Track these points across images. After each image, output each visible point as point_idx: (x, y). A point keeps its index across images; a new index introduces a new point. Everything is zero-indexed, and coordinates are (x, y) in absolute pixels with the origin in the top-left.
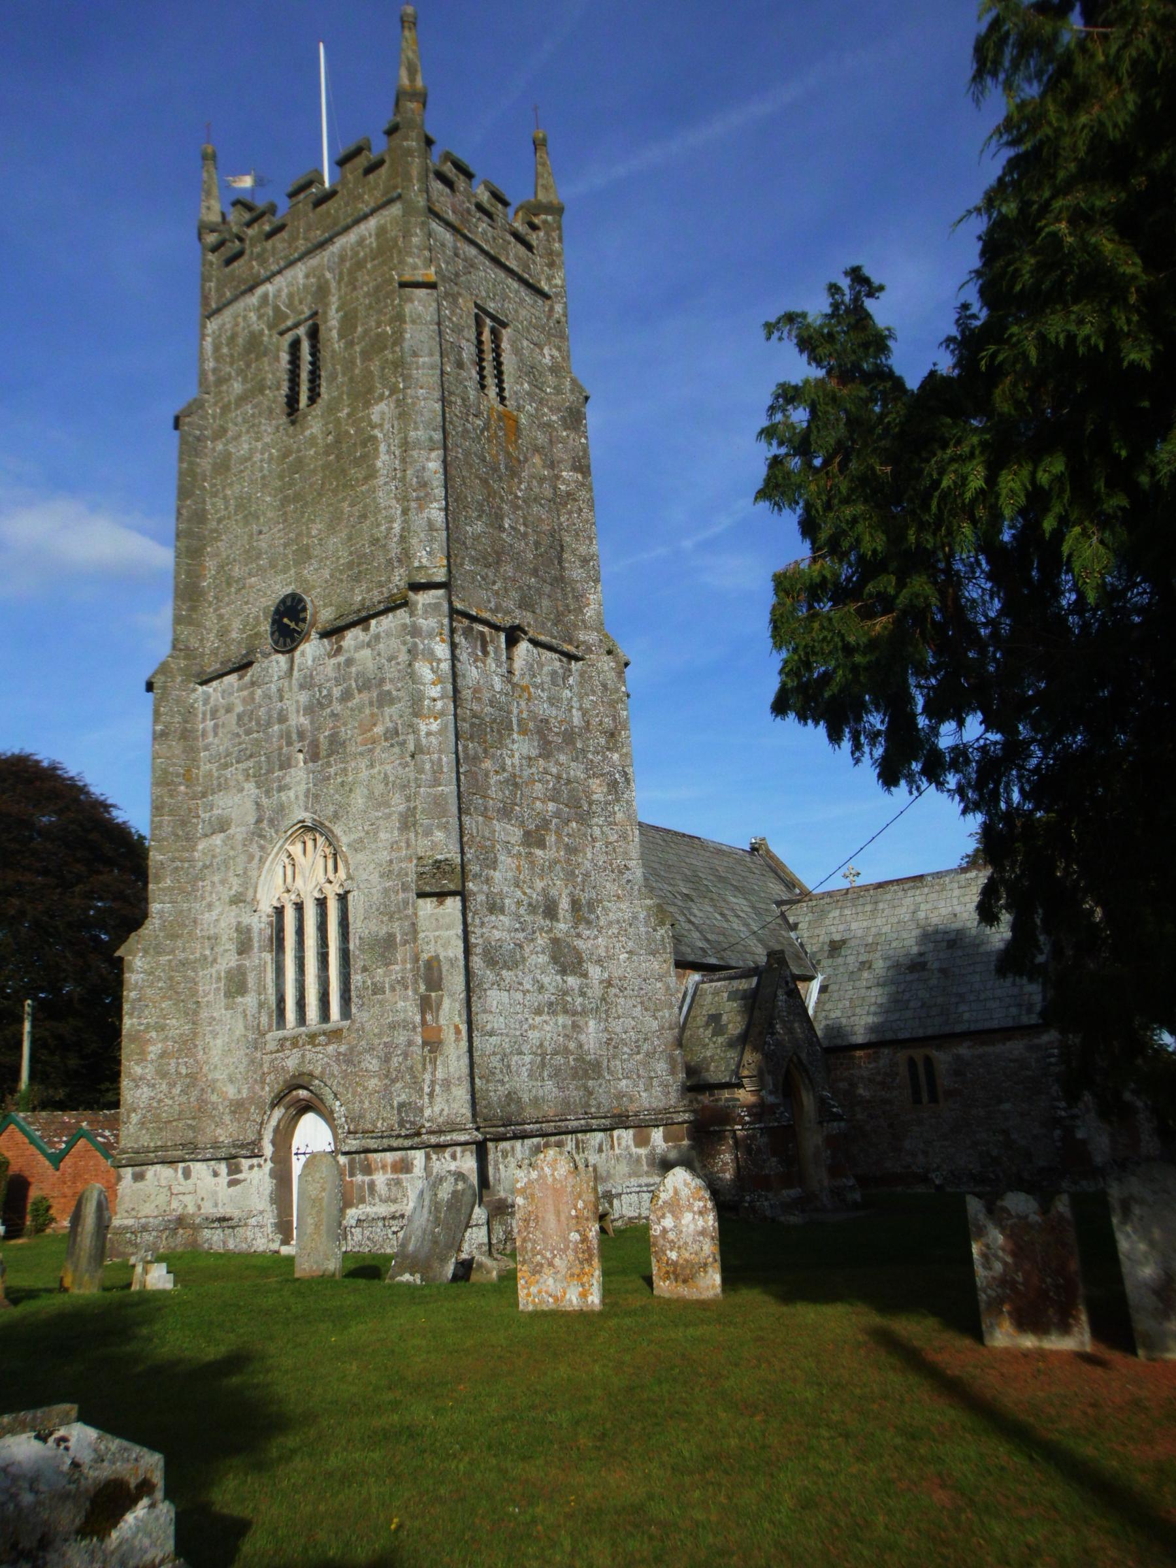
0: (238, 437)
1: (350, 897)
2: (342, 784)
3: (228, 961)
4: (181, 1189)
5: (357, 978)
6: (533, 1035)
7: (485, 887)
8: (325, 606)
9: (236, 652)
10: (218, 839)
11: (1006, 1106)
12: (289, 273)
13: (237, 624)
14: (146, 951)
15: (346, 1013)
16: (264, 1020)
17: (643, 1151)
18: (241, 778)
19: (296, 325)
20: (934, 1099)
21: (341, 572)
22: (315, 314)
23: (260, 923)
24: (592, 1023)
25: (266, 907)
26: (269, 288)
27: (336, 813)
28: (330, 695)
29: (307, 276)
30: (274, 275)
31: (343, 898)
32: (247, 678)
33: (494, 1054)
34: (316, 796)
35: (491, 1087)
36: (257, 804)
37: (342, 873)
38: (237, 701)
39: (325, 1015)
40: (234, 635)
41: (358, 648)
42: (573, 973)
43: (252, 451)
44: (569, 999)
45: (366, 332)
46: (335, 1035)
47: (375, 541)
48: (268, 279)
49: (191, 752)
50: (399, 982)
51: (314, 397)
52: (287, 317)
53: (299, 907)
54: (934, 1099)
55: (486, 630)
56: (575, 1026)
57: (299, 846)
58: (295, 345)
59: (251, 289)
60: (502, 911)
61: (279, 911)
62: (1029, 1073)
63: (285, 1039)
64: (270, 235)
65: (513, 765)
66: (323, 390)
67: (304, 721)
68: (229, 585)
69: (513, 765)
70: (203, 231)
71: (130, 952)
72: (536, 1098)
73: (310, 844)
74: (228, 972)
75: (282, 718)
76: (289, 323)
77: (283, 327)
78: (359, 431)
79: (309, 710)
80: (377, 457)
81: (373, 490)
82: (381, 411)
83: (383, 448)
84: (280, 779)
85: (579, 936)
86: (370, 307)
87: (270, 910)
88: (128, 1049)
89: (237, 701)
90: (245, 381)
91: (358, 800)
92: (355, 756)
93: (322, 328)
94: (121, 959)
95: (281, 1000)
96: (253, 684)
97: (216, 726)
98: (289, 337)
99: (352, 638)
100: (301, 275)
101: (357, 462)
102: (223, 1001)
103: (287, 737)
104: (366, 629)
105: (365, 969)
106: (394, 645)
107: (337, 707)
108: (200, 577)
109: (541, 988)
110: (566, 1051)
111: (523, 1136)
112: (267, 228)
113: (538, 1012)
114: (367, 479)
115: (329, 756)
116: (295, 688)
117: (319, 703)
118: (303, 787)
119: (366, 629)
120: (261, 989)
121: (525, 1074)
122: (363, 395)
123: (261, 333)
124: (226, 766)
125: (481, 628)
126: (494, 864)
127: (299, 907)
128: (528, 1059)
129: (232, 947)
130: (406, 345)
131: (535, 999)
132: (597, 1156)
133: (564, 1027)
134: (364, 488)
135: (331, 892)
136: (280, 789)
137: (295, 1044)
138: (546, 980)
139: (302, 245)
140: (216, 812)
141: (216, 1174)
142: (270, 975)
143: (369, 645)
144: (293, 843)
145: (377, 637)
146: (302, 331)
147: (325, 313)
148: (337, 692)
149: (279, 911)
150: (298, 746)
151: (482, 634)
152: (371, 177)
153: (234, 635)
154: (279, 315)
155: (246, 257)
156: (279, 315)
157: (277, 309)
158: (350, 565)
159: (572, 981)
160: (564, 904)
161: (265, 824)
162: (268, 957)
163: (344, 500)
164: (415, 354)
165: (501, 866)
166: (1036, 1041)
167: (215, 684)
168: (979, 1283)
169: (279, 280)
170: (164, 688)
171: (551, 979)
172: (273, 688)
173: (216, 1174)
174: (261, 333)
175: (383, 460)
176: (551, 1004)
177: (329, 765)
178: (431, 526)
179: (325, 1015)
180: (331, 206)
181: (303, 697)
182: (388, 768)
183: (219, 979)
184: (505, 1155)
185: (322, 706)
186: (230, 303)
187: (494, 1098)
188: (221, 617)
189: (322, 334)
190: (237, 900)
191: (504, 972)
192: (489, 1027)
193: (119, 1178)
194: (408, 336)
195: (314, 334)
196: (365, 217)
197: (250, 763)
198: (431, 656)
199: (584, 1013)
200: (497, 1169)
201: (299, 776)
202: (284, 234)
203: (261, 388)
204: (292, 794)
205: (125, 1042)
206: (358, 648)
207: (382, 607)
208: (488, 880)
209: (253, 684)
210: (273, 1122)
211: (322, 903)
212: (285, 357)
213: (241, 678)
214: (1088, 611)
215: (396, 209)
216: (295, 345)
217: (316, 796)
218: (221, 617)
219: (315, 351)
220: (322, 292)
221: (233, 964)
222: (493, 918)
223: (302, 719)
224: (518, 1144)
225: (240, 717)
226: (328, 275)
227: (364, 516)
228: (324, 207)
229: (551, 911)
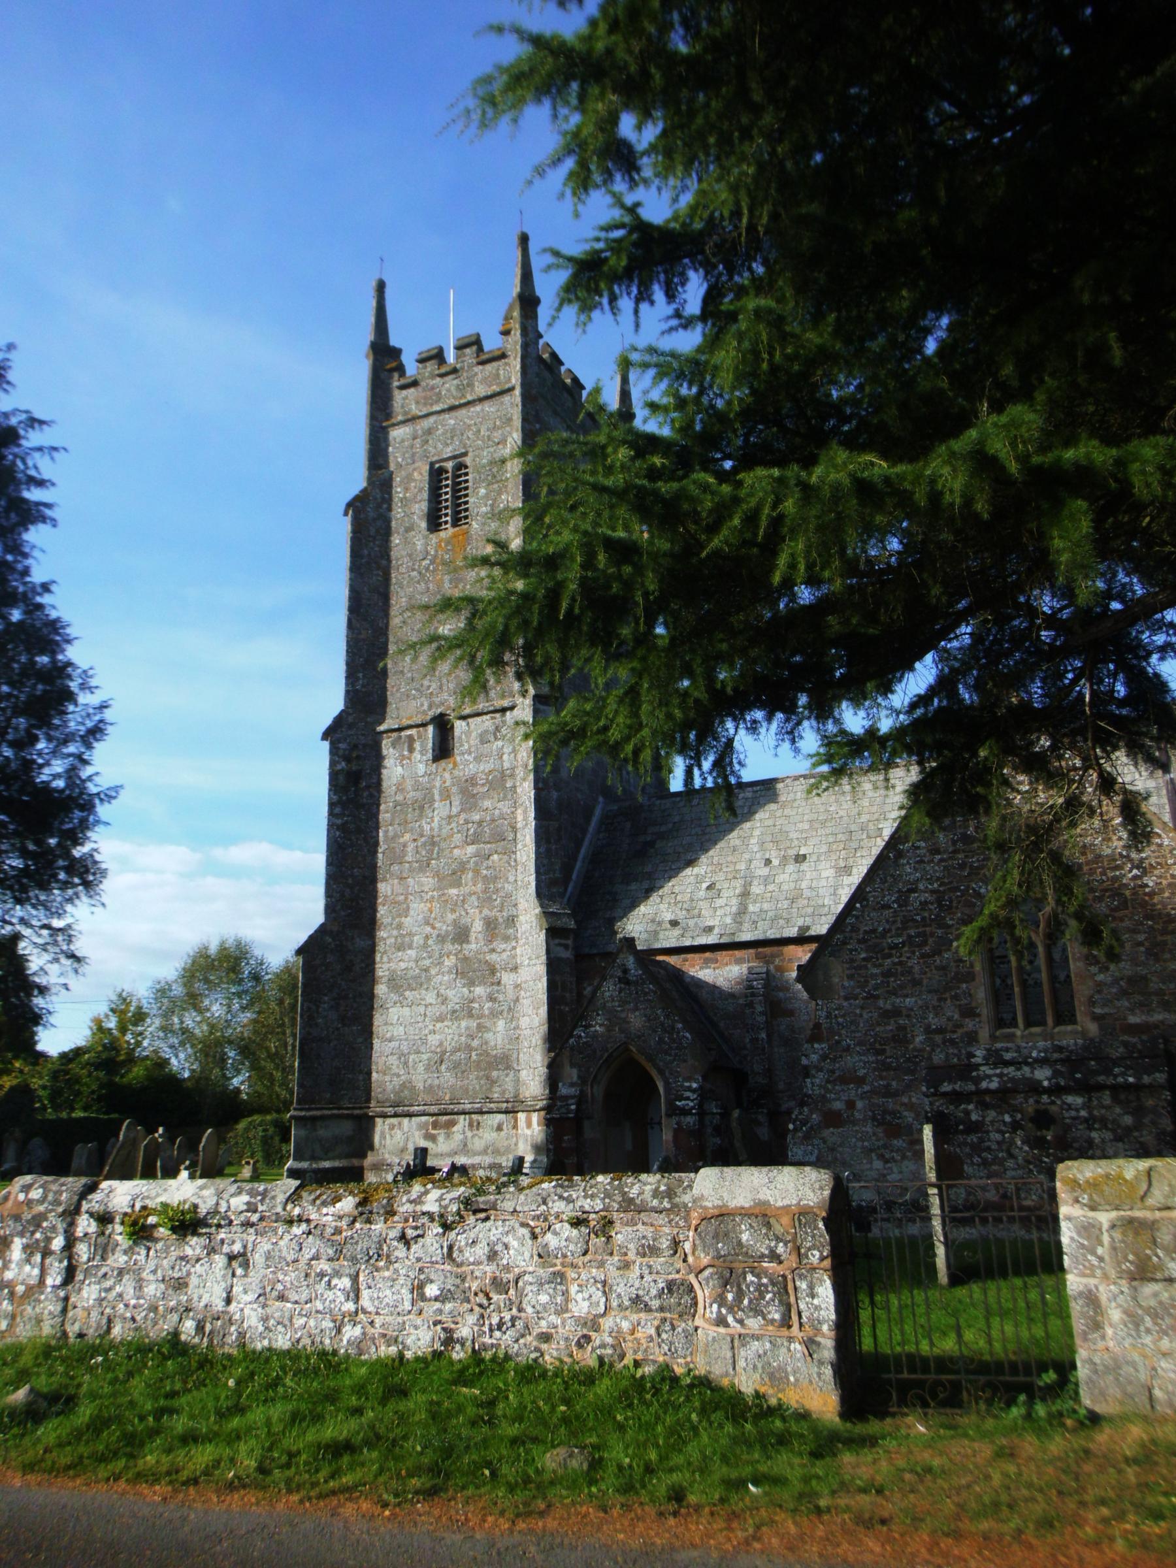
6: (434, 1040)
7: (395, 933)
35: (387, 1078)
44: (476, 1005)
50: (981, 1140)
56: (480, 1027)
65: (432, 829)
69: (432, 829)
70: (484, 357)
72: (431, 1086)
85: (493, 950)
109: (445, 1001)
110: (469, 1048)
111: (410, 1115)
121: (421, 1068)
125: (409, 732)
132: (494, 1135)
138: (450, 993)
160: (478, 926)
165: (412, 912)
168: (1069, 1292)
176: (454, 1012)
184: (392, 1127)
187: (389, 1087)
191: (407, 993)
200: (383, 1137)
208: (400, 926)
214: (843, 433)
224: (406, 1121)
229: (462, 935)
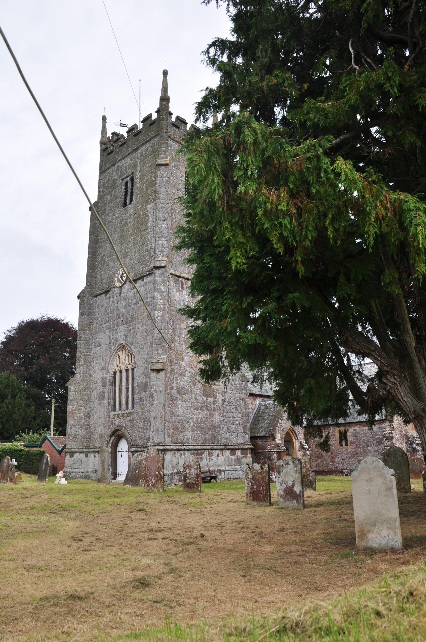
0: (108, 214)
1: (135, 369)
2: (134, 332)
3: (100, 389)
4: (85, 460)
5: (136, 396)
8: (131, 272)
9: (105, 287)
10: (98, 348)
11: (370, 448)
12: (126, 159)
13: (106, 277)
14: (75, 384)
15: (133, 407)
16: (110, 408)
17: (233, 457)
18: (105, 328)
19: (127, 177)
20: (346, 445)
21: (137, 261)
22: (133, 173)
23: (109, 377)
24: (217, 414)
25: (111, 371)
26: (120, 164)
27: (132, 341)
28: (131, 302)
29: (131, 160)
30: (121, 160)
31: (133, 369)
32: (108, 296)
33: (179, 422)
34: (126, 335)
36: (110, 338)
37: (133, 362)
38: (105, 303)
39: (127, 408)
40: (105, 281)
41: (140, 287)
42: (211, 397)
43: (112, 219)
45: (148, 180)
46: (129, 414)
47: (147, 251)
48: (120, 161)
49: (91, 320)
51: (131, 201)
52: (124, 174)
53: (121, 372)
54: (346, 445)
55: (183, 280)
56: (210, 414)
57: (121, 352)
58: (127, 183)
59: (114, 165)
60: (185, 375)
61: (115, 373)
62: (378, 436)
63: (115, 415)
64: (121, 146)
66: (134, 199)
67: (124, 311)
68: (104, 264)
71: (70, 384)
73: (124, 351)
74: (100, 392)
75: (118, 310)
76: (125, 176)
77: (123, 177)
78: (144, 213)
79: (125, 307)
80: (148, 222)
81: (147, 234)
82: (150, 207)
83: (150, 219)
84: (117, 330)
86: (149, 171)
87: (112, 373)
88: (69, 416)
89: (105, 303)
90: (112, 196)
91: (139, 337)
92: (138, 323)
93: (134, 178)
94: (67, 387)
95: (115, 403)
96: (110, 298)
97: (98, 311)
98: (125, 181)
99: (139, 284)
100: (129, 160)
101: (142, 224)
102: (98, 402)
103: (118, 315)
104: (143, 280)
105: (138, 393)
106: (150, 286)
107: (133, 306)
108: (96, 261)
112: (120, 143)
113: (197, 409)
114: (145, 230)
115: (131, 322)
116: (122, 299)
117: (129, 305)
118: (123, 333)
119: (143, 280)
120: (109, 398)
122: (146, 202)
123: (117, 179)
124: (101, 325)
125: (181, 279)
126: (183, 359)
127: (121, 372)
128: (192, 424)
129: (101, 384)
130: (157, 185)
131: (195, 404)
133: (206, 414)
134: (145, 232)
135: (130, 367)
136: (116, 333)
137: (118, 417)
139: (130, 149)
140: (98, 340)
141: (95, 457)
142: (112, 394)
143: (143, 286)
144: (120, 351)
145: (146, 283)
146: (128, 179)
147: (136, 173)
148: (133, 301)
149: (115, 373)
150: (122, 319)
151: (182, 282)
152: (151, 127)
153: (105, 281)
154: (122, 173)
155: (113, 153)
156: (122, 173)
157: (121, 171)
158: (140, 259)
159: (211, 400)
161: (111, 344)
162: (111, 388)
163: (138, 236)
164: (160, 188)
166: (381, 426)
167: (99, 297)
169: (123, 162)
170: (83, 298)
171: (201, 398)
172: (115, 299)
173: (95, 457)
174: (117, 179)
175: (150, 224)
176: (202, 407)
177: (130, 325)
178: (163, 247)
179: (127, 408)
180: (140, 136)
181: (124, 303)
182: (148, 327)
183: (97, 394)
185: (129, 306)
186: (108, 168)
188: (101, 275)
189: (135, 181)
190: (102, 369)
192: (177, 414)
193: (66, 456)
194: (158, 182)
195: (132, 180)
196: (149, 141)
197: (107, 324)
198: (161, 292)
199: (214, 410)
201: (122, 329)
202: (125, 146)
203: (116, 197)
204: (120, 334)
205: (68, 413)
206: (140, 287)
207: (147, 273)
208: (180, 365)
209: (110, 298)
210: (111, 441)
211: (127, 371)
212: (123, 187)
213: (106, 295)
215: (157, 139)
216: (127, 183)
217: (126, 335)
218: (101, 275)
219: (132, 186)
220: (135, 166)
221: (101, 390)
222: (181, 378)
223: (123, 310)
225: (106, 308)
226: (137, 160)
227: (144, 243)
228: (137, 137)
